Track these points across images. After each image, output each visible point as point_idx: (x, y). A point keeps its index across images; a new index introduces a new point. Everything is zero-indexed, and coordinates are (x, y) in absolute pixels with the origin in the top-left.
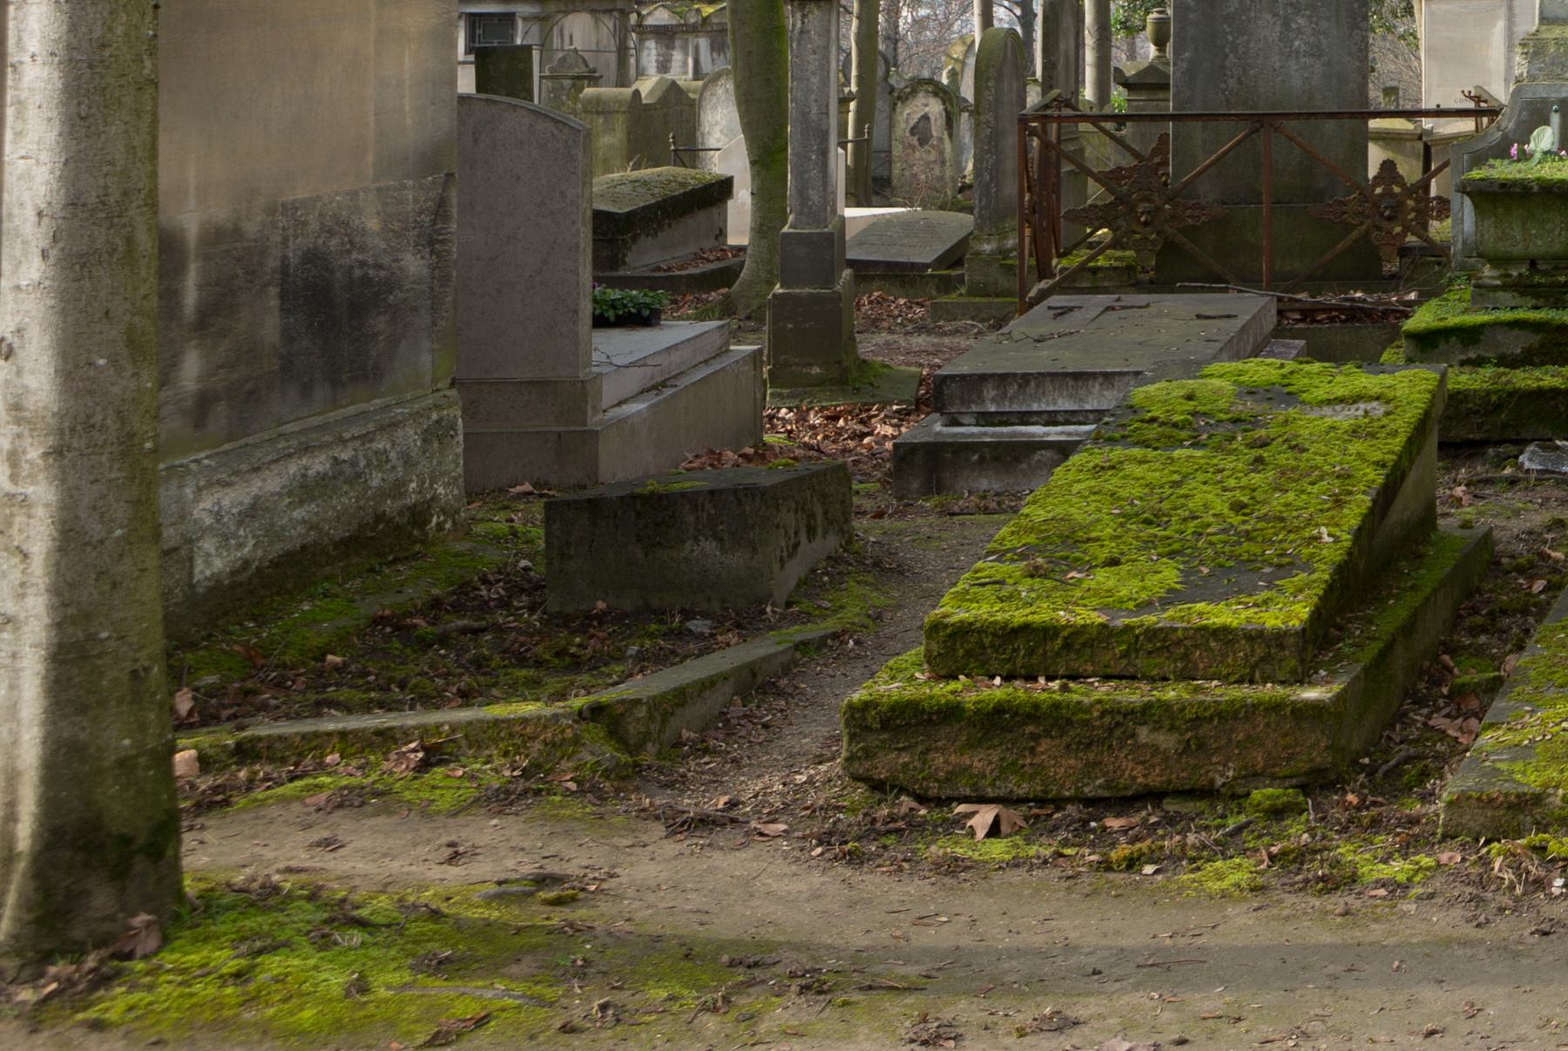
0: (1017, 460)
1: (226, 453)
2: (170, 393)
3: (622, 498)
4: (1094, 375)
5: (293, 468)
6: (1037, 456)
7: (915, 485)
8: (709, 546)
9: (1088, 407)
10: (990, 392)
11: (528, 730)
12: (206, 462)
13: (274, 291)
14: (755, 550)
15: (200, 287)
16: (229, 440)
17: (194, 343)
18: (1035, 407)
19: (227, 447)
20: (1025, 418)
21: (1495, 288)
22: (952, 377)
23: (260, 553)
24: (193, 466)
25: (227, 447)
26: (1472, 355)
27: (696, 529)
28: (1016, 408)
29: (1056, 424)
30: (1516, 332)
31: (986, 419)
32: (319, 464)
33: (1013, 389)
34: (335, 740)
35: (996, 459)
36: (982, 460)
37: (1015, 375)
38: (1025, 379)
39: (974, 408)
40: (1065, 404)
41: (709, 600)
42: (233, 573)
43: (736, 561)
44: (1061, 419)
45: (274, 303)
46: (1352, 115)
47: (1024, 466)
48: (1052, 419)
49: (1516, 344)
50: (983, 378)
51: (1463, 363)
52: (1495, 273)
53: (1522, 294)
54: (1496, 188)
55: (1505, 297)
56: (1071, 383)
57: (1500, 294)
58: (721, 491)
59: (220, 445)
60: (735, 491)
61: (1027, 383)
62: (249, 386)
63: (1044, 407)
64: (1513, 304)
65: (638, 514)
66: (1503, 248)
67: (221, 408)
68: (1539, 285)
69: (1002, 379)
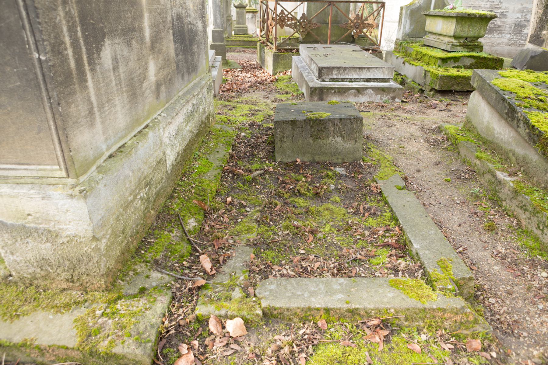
0: (345, 92)
1: (167, 109)
2: (147, 83)
3: (305, 120)
4: (365, 68)
5: (185, 111)
6: (350, 91)
7: (316, 99)
8: (339, 139)
9: (362, 77)
10: (335, 72)
11: (446, 315)
12: (162, 114)
13: (171, 31)
14: (356, 141)
15: (151, 26)
16: (167, 103)
17: (151, 57)
18: (347, 77)
19: (167, 106)
20: (343, 80)
21: (457, 46)
22: (325, 68)
23: (181, 147)
24: (159, 118)
25: (167, 106)
26: (456, 65)
27: (334, 133)
28: (342, 77)
29: (352, 82)
30: (469, 59)
31: (333, 80)
32: (189, 107)
33: (341, 71)
34: (322, 313)
35: (339, 92)
36: (335, 92)
37: (342, 67)
38: (345, 68)
39: (330, 77)
40: (356, 76)
41: (338, 158)
42: (176, 160)
43: (349, 145)
44: (353, 80)
45: (172, 38)
46: (346, 2)
47: (346, 94)
48: (351, 80)
49: (468, 62)
50: (333, 68)
51: (453, 67)
52: (457, 41)
53: (464, 48)
54: (467, 16)
55: (459, 48)
56: (358, 70)
57: (458, 47)
58: (344, 119)
59: (165, 106)
60: (350, 119)
61: (346, 70)
62: (169, 77)
63: (350, 77)
64: (461, 50)
65: (311, 126)
66: (462, 34)
67: (163, 88)
68: (470, 45)
69: (339, 68)
